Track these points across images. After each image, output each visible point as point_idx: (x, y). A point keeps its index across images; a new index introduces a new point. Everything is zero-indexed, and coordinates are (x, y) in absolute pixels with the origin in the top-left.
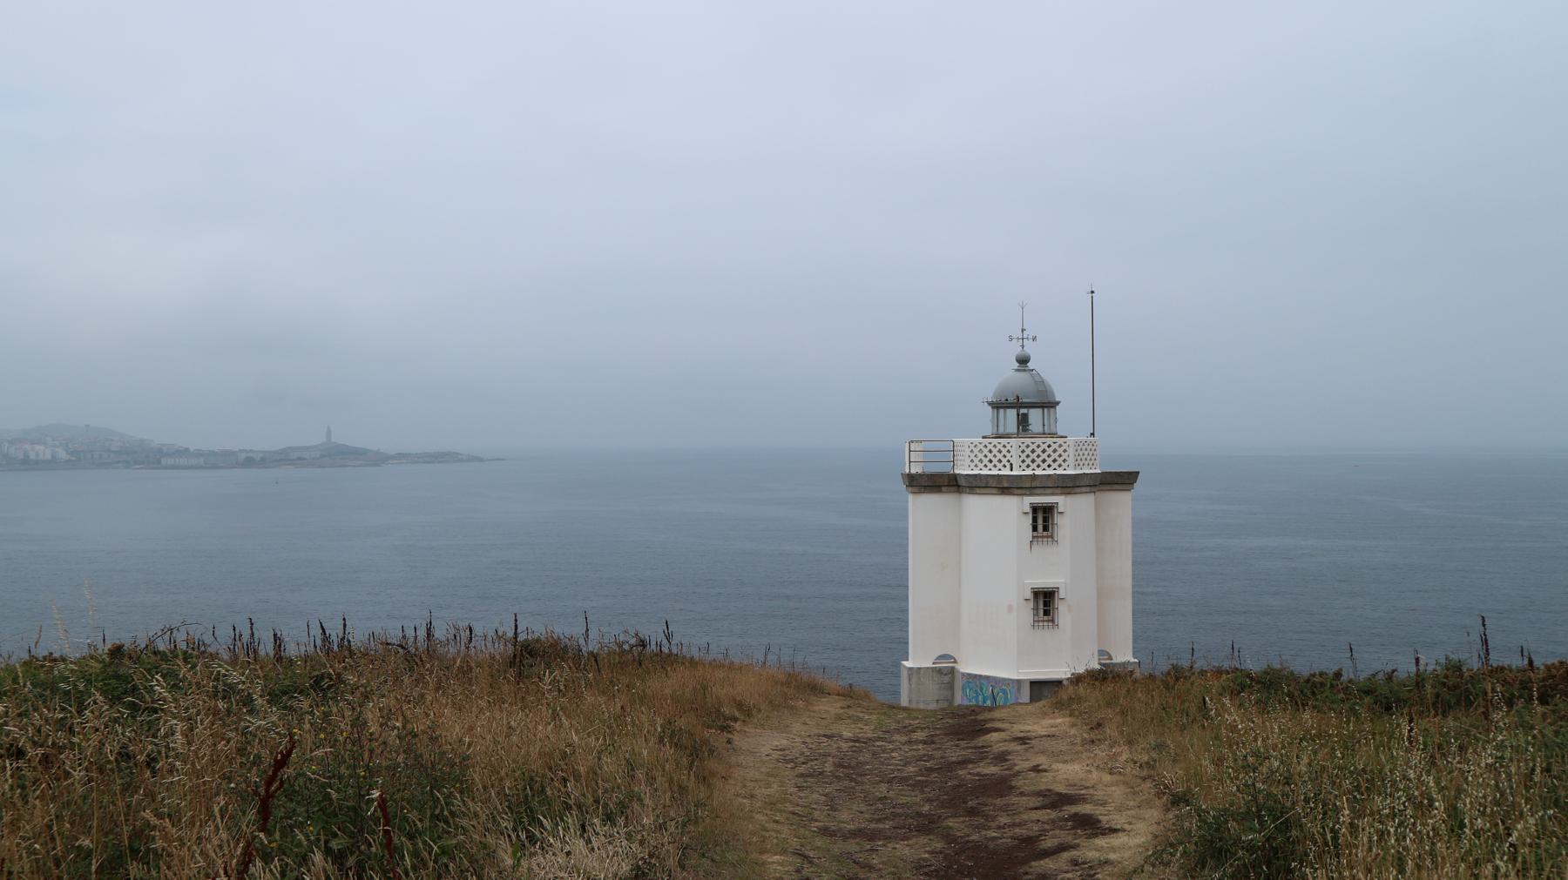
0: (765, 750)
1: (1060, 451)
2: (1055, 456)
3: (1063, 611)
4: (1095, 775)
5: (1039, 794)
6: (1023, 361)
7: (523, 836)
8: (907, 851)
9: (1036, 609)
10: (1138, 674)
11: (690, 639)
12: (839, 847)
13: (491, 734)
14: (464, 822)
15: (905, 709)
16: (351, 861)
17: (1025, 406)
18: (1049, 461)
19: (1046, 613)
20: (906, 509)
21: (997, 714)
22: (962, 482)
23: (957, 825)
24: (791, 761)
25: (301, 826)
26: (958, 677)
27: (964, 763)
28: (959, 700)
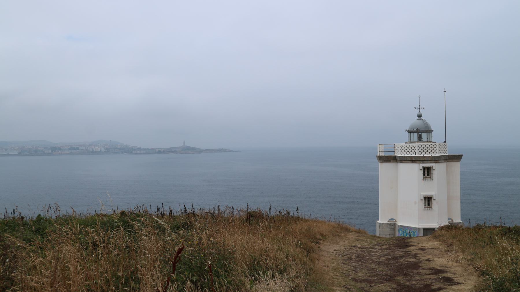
0: (331, 250)
1: (433, 147)
2: (432, 149)
3: (435, 204)
4: (450, 263)
5: (430, 269)
6: (420, 116)
7: (253, 278)
8: (383, 287)
9: (425, 203)
10: (464, 227)
11: (305, 213)
12: (359, 285)
13: (243, 243)
14: (234, 273)
15: (379, 237)
16: (199, 284)
17: (421, 132)
18: (429, 151)
19: (429, 204)
20: (378, 168)
21: (412, 240)
22: (398, 159)
23: (399, 278)
24: (340, 255)
25: (184, 272)
26: (397, 227)
27: (402, 257)
28: (397, 235)
